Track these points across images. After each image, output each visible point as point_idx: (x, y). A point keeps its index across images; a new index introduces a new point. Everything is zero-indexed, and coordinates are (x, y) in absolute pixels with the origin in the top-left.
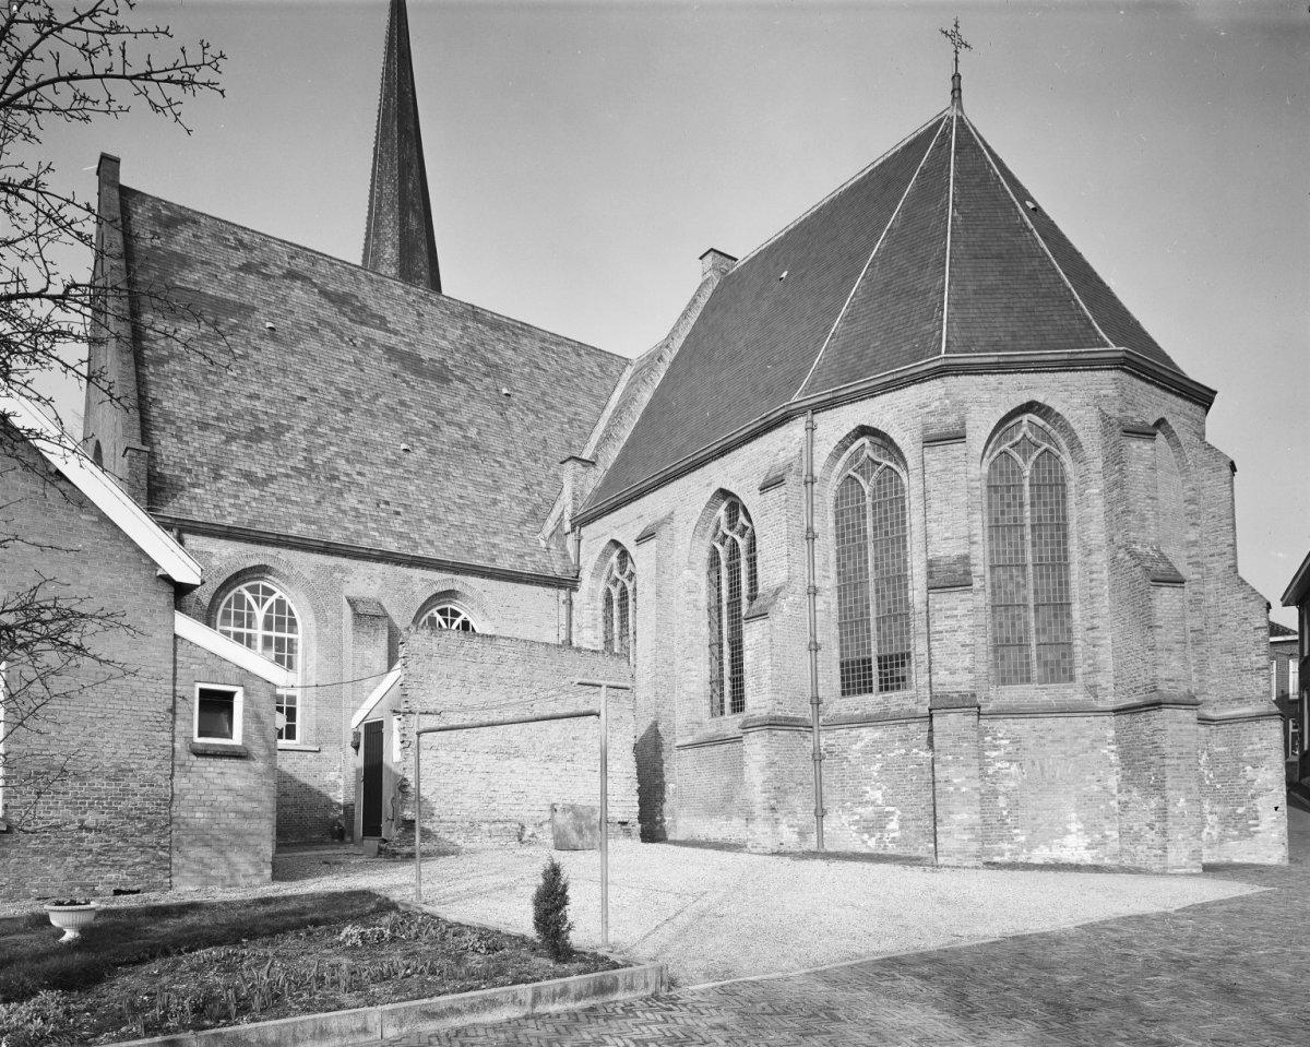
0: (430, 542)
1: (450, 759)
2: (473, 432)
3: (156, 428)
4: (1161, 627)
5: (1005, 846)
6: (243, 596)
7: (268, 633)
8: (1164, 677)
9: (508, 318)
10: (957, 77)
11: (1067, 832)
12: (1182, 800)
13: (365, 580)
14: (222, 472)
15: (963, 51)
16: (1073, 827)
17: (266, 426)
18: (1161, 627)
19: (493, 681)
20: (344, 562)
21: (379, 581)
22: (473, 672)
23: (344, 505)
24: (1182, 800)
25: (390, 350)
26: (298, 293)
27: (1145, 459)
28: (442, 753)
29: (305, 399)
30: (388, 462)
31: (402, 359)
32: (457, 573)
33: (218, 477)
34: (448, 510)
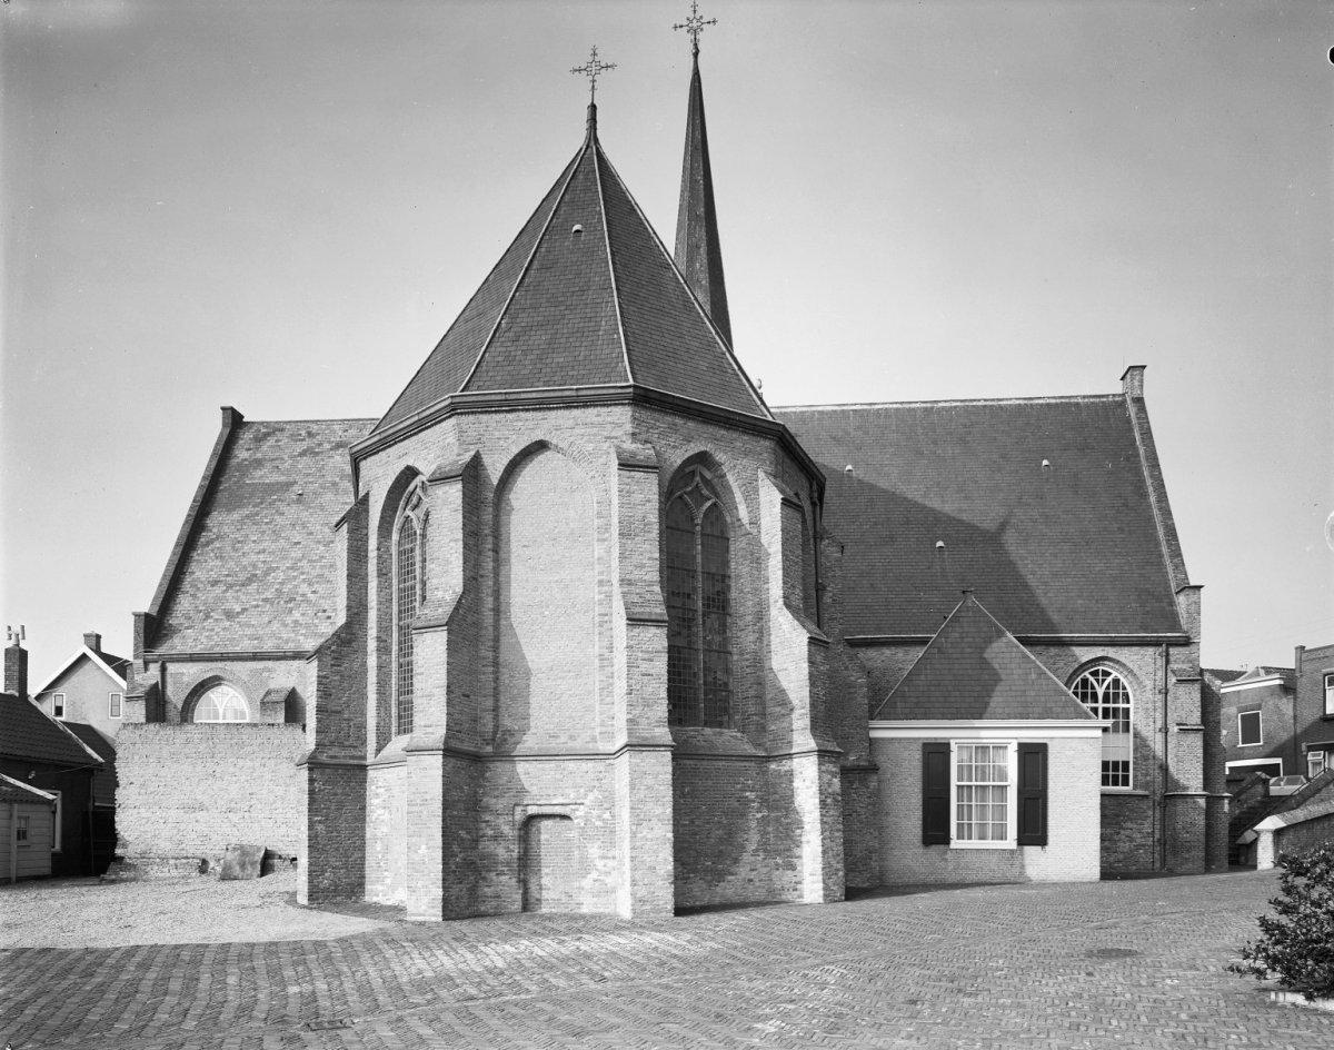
1: (149, 814)
4: (422, 674)
6: (1087, 679)
7: (1106, 705)
8: (422, 724)
10: (593, 108)
12: (423, 847)
18: (422, 674)
20: (270, 664)
22: (165, 753)
23: (289, 620)
24: (423, 847)
28: (142, 810)
33: (207, 617)
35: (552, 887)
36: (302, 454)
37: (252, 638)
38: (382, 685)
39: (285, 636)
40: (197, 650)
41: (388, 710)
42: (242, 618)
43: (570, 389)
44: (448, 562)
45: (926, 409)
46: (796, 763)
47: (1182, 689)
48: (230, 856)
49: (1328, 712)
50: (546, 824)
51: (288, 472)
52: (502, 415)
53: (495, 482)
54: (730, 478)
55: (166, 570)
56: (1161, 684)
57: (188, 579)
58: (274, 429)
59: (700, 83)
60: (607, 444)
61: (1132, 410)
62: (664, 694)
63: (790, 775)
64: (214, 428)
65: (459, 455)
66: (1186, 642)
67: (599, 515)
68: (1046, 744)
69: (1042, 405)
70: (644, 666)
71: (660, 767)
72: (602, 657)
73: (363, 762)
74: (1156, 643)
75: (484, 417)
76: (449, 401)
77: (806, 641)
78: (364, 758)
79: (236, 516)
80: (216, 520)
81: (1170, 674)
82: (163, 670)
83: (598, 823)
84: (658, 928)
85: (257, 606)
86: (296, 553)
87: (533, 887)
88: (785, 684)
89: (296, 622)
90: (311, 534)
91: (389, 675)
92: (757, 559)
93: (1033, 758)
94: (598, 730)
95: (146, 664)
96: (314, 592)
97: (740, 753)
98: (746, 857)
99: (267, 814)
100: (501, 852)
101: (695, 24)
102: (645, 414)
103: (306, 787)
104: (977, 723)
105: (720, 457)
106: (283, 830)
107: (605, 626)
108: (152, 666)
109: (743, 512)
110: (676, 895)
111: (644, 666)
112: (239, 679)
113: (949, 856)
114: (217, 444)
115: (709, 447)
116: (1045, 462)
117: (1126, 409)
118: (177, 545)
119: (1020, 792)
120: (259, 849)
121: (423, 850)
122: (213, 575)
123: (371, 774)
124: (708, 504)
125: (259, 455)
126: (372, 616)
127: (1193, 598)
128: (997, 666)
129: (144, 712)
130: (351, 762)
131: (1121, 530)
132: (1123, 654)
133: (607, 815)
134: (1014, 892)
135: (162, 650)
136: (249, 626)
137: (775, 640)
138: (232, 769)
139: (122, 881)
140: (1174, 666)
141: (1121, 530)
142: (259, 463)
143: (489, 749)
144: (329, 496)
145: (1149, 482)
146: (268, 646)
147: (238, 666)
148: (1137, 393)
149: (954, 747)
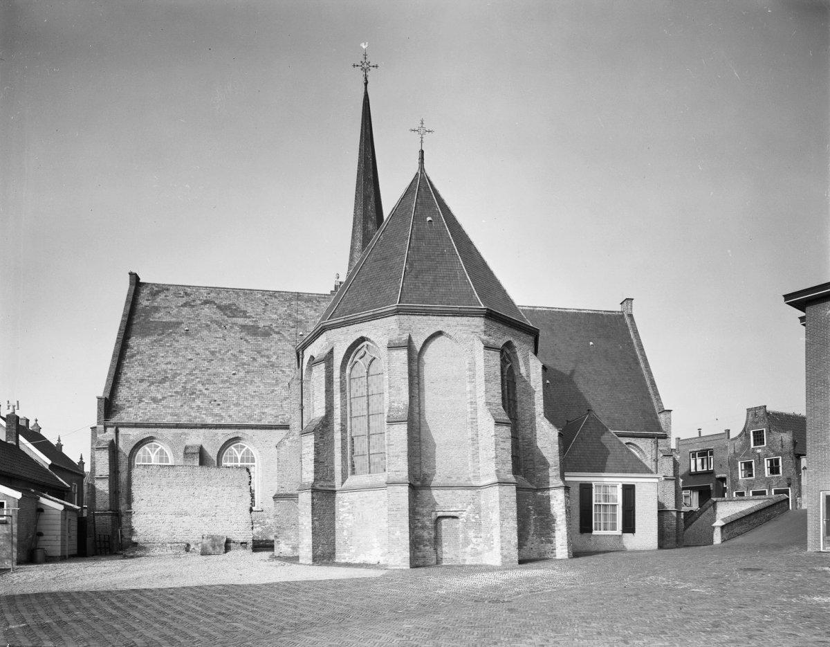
0: (230, 416)
2: (273, 359)
3: (121, 385)
5: (346, 554)
8: (394, 470)
9: (317, 294)
11: (373, 547)
12: (398, 532)
13: (195, 438)
14: (143, 399)
15: (427, 137)
16: (375, 545)
17: (169, 376)
19: (174, 484)
20: (186, 431)
21: (202, 437)
22: (164, 482)
23: (194, 405)
24: (398, 532)
25: (243, 327)
26: (207, 310)
27: (401, 360)
28: (149, 515)
29: (192, 360)
30: (223, 382)
31: (248, 329)
32: (239, 429)
33: (141, 401)
34: (246, 399)
35: (448, 552)
36: (185, 305)
37: (172, 415)
38: (344, 448)
39: (193, 414)
40: (138, 420)
41: (346, 462)
42: (163, 402)
43: (438, 306)
44: (399, 389)
45: (530, 310)
46: (551, 492)
47: (665, 459)
48: (205, 541)
49: (698, 470)
50: (444, 521)
51: (176, 316)
52: (421, 317)
53: (418, 350)
54: (519, 354)
55: (110, 371)
56: (654, 457)
57: (123, 378)
58: (163, 289)
59: (368, 100)
60: (473, 335)
61: (628, 321)
62: (510, 458)
63: (548, 498)
64: (124, 287)
65: (399, 335)
66: (665, 437)
67: (470, 370)
68: (634, 485)
69: (585, 313)
70: (502, 445)
71: (511, 492)
72: (473, 439)
73: (334, 489)
74: (652, 437)
75: (412, 317)
76: (396, 307)
77: (557, 434)
78: (334, 487)
79: (147, 340)
80: (134, 341)
81: (659, 452)
82: (117, 432)
83: (474, 520)
84: (512, 569)
85: (171, 396)
86: (191, 365)
87: (439, 552)
88: (545, 455)
89: (199, 406)
90: (198, 354)
91: (346, 443)
92: (530, 393)
93: (629, 491)
94: (472, 474)
95: (105, 428)
96: (206, 389)
97: (524, 487)
98: (530, 537)
99: (226, 518)
100: (425, 534)
101: (365, 66)
102: (489, 322)
103: (310, 502)
104: (603, 474)
105: (516, 343)
106: (235, 526)
107: (475, 424)
108: (109, 429)
109: (523, 370)
110: (519, 554)
111: (502, 445)
112: (166, 439)
113: (592, 538)
114: (128, 295)
115: (511, 339)
116: (591, 343)
117: (624, 320)
118: (114, 356)
119: (623, 507)
120: (223, 537)
121: (398, 533)
122: (140, 375)
123: (338, 495)
124: (509, 365)
125: (156, 304)
126: (337, 413)
127: (668, 416)
128: (608, 447)
129: (108, 457)
130: (329, 489)
131: (630, 380)
132: (638, 442)
133: (477, 517)
134: (620, 554)
135: (115, 420)
136: (169, 407)
137: (539, 433)
138: (204, 492)
139: (138, 556)
140: (660, 448)
141: (630, 380)
142: (157, 309)
143: (419, 483)
144: (205, 333)
145: (640, 357)
146: (184, 420)
147: (165, 431)
148: (629, 312)
149: (594, 486)
